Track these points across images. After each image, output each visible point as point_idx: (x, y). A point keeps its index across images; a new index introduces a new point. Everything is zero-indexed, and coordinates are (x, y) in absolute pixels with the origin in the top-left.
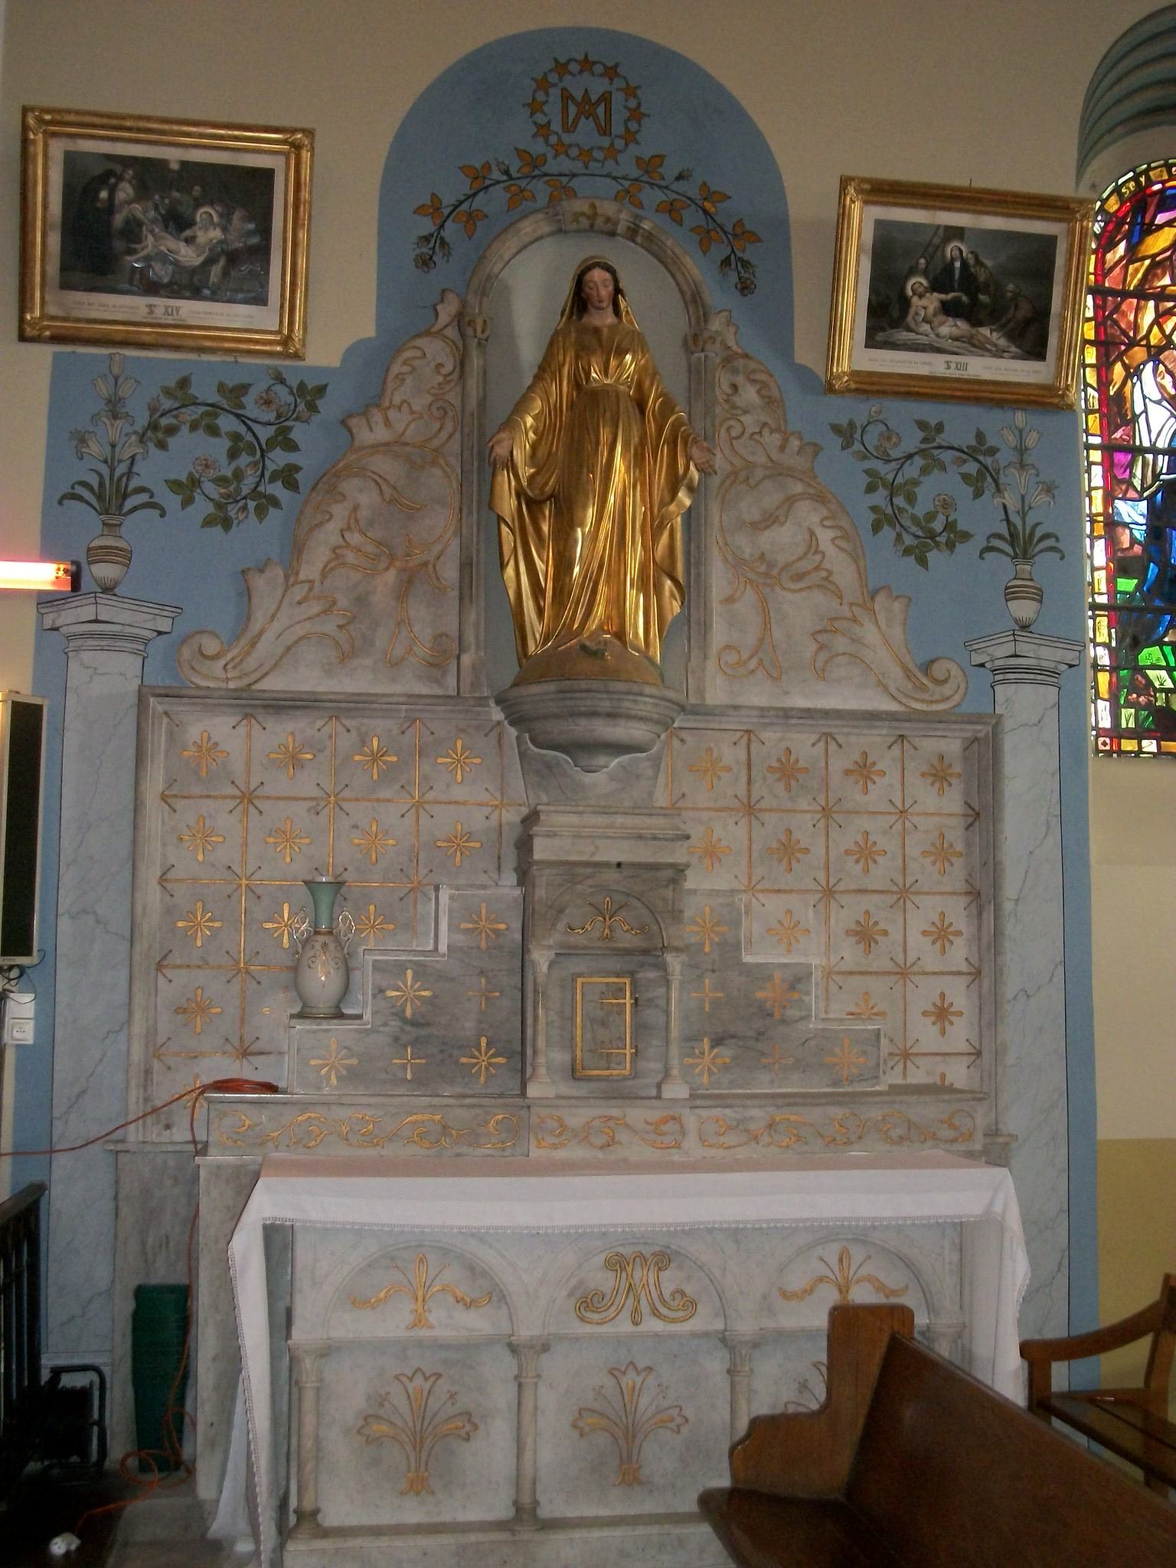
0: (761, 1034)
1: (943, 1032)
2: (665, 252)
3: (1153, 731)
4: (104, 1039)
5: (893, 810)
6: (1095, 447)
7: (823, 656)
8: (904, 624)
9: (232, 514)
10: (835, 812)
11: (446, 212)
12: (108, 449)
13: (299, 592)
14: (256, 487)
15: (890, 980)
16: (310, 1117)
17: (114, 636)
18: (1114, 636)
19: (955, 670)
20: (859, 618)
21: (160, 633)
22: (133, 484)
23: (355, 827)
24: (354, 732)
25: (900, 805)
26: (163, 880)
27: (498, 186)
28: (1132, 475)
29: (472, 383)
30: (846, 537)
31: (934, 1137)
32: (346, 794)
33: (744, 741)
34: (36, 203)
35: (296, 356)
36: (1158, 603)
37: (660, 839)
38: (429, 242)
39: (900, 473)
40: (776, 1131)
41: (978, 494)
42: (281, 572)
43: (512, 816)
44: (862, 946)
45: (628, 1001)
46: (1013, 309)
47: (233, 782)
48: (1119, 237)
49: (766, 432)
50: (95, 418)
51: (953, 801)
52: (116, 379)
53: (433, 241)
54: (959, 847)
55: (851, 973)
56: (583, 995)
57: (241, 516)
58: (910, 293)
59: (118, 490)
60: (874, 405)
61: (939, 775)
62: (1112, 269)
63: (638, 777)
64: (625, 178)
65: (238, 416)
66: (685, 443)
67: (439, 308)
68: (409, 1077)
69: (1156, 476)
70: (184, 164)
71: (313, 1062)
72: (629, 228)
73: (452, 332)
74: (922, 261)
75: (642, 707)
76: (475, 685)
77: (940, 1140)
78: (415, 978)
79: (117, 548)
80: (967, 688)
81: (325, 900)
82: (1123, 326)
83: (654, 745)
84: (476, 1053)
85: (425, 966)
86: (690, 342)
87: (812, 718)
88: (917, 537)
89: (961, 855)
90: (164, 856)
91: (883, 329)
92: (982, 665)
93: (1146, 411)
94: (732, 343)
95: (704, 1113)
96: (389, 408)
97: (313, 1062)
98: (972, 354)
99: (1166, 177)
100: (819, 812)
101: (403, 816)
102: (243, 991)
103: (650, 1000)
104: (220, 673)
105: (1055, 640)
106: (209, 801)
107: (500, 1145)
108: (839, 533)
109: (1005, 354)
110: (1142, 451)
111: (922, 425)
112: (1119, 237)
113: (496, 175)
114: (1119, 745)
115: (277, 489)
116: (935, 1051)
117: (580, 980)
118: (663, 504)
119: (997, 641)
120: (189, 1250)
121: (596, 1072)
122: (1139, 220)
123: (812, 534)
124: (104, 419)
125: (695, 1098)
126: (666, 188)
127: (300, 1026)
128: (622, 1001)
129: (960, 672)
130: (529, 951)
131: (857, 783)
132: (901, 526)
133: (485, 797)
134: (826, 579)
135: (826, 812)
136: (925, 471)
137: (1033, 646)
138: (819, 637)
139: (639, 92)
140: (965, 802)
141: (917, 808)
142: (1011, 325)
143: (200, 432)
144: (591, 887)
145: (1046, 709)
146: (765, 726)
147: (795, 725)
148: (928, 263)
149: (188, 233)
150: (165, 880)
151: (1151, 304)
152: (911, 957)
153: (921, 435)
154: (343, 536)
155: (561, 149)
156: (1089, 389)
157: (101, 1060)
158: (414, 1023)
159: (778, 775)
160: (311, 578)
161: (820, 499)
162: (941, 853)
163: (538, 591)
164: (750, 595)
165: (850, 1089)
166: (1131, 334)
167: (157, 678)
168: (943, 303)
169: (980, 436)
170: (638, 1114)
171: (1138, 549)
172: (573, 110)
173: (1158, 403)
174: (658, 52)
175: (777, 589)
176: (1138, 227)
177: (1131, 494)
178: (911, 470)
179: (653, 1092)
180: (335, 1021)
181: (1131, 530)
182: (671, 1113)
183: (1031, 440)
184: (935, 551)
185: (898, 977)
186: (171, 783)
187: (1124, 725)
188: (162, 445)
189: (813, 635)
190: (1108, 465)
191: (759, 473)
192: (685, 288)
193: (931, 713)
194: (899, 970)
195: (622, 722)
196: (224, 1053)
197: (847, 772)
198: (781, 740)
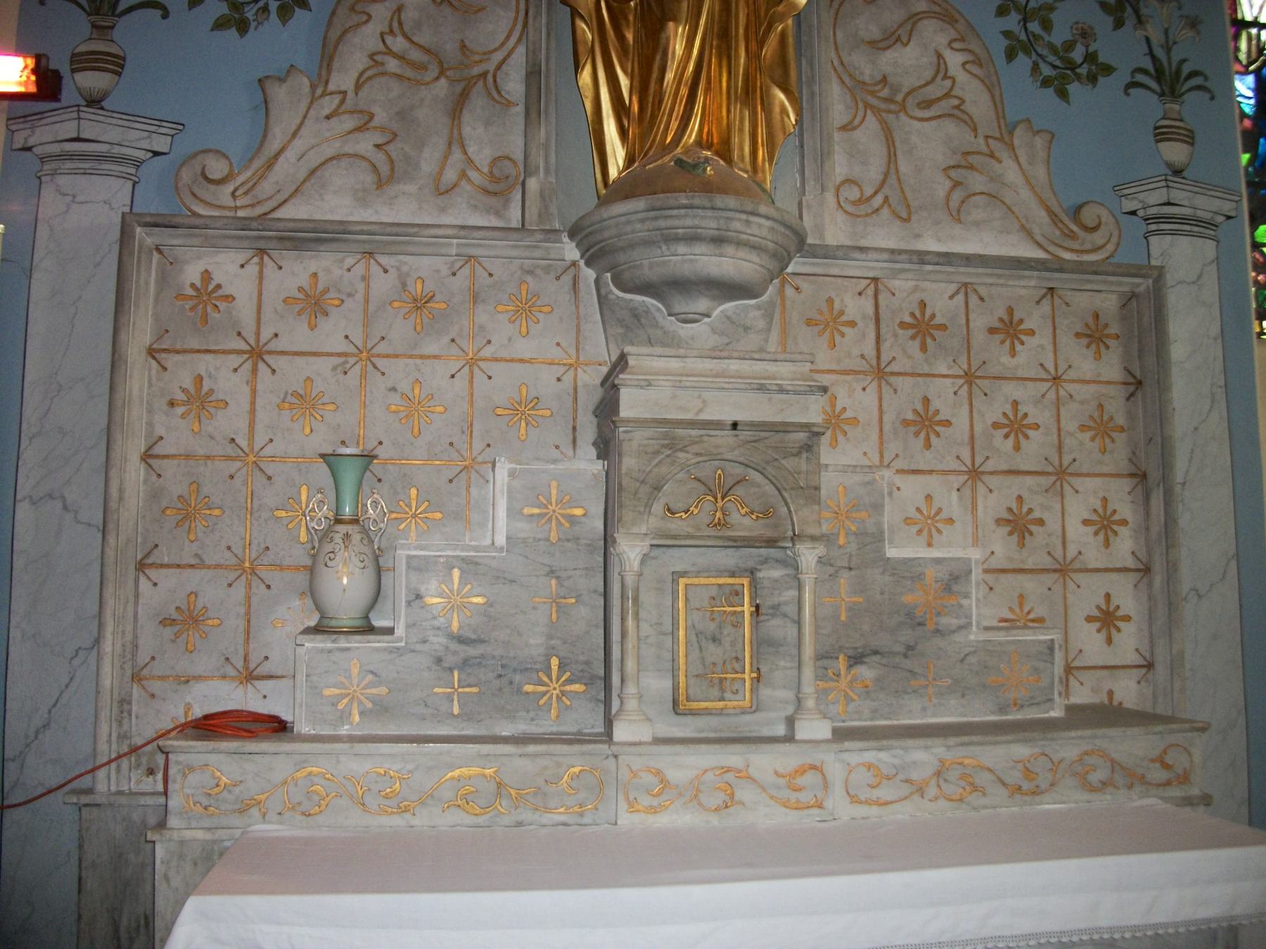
0: (910, 648)
1: (1109, 641)
4: (72, 658)
5: (1044, 376)
7: (957, 196)
8: (1048, 163)
13: (329, 104)
15: (1048, 579)
16: (310, 774)
17: (99, 158)
20: (997, 154)
21: (156, 154)
23: (394, 389)
24: (393, 273)
25: (1053, 371)
26: (147, 457)
30: (978, 62)
31: (1142, 780)
32: (382, 348)
33: (870, 291)
37: (787, 392)
40: (946, 780)
41: (1119, 24)
42: (306, 82)
43: (591, 378)
44: (1015, 537)
45: (747, 609)
47: (239, 334)
51: (1111, 367)
54: (1121, 420)
55: (1003, 571)
56: (687, 600)
61: (1094, 335)
68: (456, 711)
71: (327, 692)
75: (756, 231)
76: (544, 215)
77: (1150, 784)
78: (463, 580)
79: (108, 54)
81: (349, 477)
83: (766, 289)
84: (545, 679)
85: (477, 564)
87: (950, 264)
88: (1055, 67)
89: (1122, 429)
90: (150, 424)
92: (1134, 213)
95: (854, 758)
97: (327, 692)
101: (453, 376)
102: (248, 598)
103: (776, 607)
104: (229, 202)
106: (208, 357)
107: (576, 809)
108: (970, 58)
116: (1101, 663)
117: (682, 581)
121: (704, 705)
123: (939, 56)
125: (841, 735)
127: (314, 643)
128: (739, 609)
129: (1111, 219)
130: (614, 541)
131: (1003, 342)
132: (1037, 54)
133: (556, 353)
134: (957, 107)
135: (969, 377)
137: (1188, 194)
138: (953, 173)
140: (1126, 369)
141: (1072, 374)
144: (697, 454)
146: (895, 274)
150: (151, 456)
152: (1072, 551)
154: (384, 41)
157: (67, 686)
158: (461, 640)
159: (911, 332)
160: (343, 88)
162: (1101, 427)
164: (871, 122)
165: (1019, 717)
167: (150, 204)
170: (765, 762)
175: (902, 116)
179: (781, 730)
180: (358, 637)
182: (809, 761)
184: (1076, 83)
185: (1057, 575)
186: (163, 333)
189: (944, 170)
193: (1081, 263)
194: (1057, 566)
195: (730, 250)
196: (224, 677)
197: (992, 331)
198: (915, 289)
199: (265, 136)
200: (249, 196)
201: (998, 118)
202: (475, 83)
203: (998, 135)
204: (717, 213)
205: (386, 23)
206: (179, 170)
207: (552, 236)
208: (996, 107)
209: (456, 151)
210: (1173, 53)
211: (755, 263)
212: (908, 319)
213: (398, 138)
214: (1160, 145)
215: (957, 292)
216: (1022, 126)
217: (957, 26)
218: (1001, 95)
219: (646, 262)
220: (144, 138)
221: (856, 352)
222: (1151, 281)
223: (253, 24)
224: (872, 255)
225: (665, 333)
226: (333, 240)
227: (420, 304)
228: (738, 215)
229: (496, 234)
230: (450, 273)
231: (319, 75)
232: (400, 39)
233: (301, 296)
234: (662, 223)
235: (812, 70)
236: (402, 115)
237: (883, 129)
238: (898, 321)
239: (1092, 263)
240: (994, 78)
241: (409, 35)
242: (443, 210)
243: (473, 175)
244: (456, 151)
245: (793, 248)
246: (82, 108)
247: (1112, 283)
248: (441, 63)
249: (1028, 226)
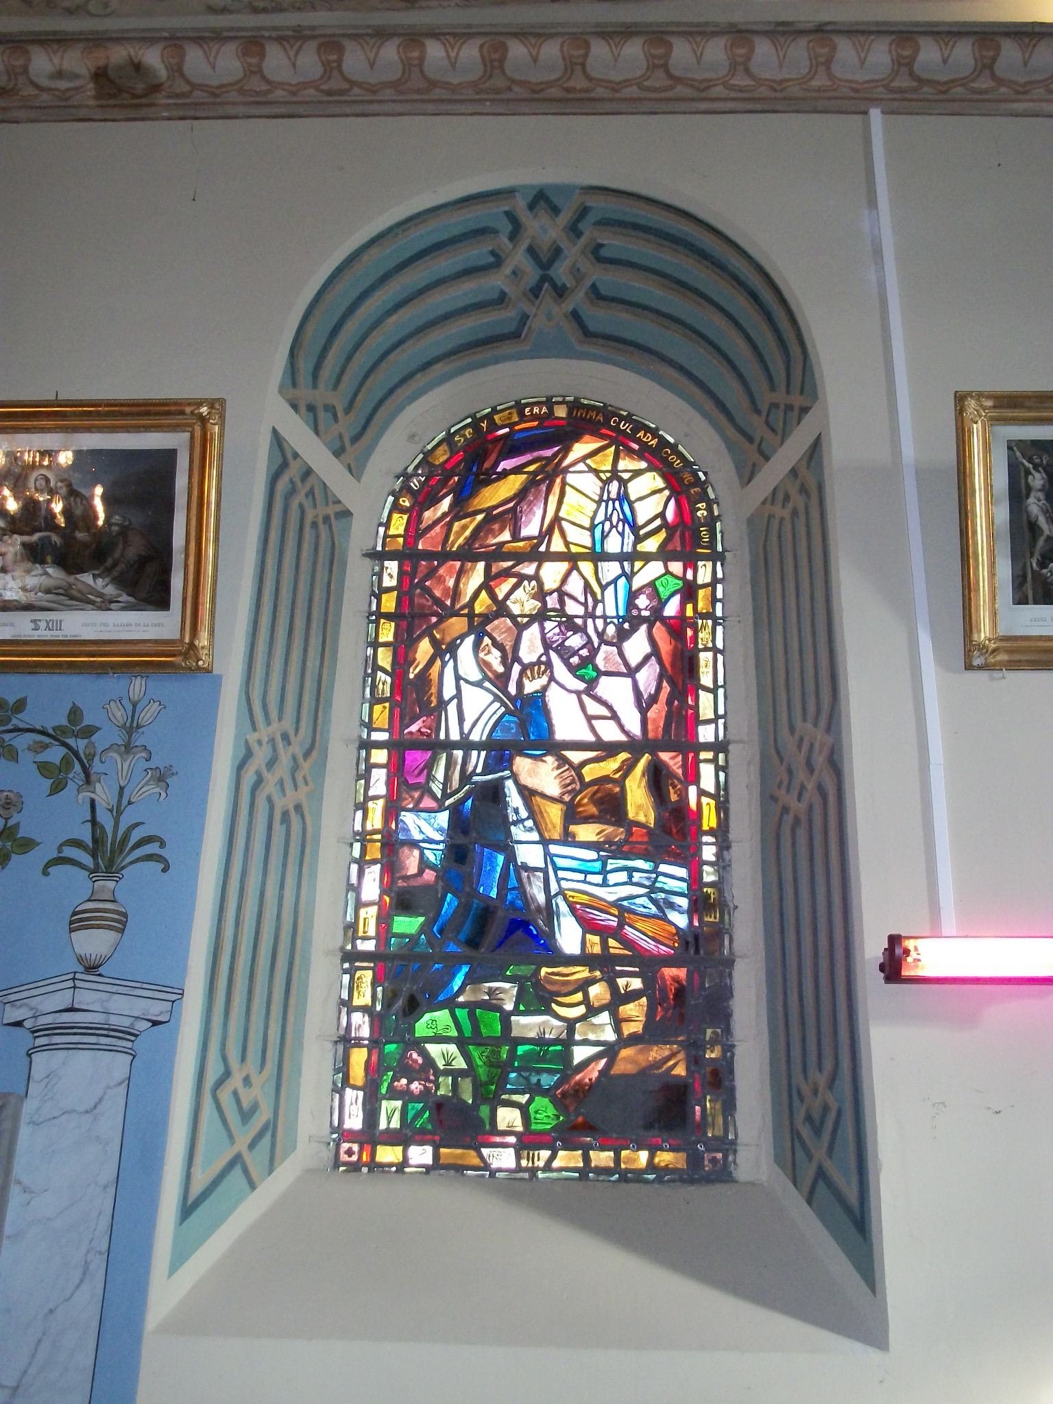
3: (430, 1132)
6: (379, 745)
18: (380, 995)
28: (430, 777)
36: (452, 948)
46: (121, 546)
48: (445, 491)
62: (430, 528)
69: (465, 778)
82: (438, 593)
92: (19, 1024)
93: (458, 695)
98: (70, 608)
99: (515, 418)
105: (130, 985)
109: (113, 606)
110: (449, 746)
112: (445, 491)
114: (373, 1154)
122: (475, 469)
145: (109, 1087)
151: (481, 566)
156: (379, 674)
166: (448, 603)
171: (429, 876)
173: (478, 684)
177: (428, 802)
181: (422, 850)
183: (146, 716)
187: (383, 1125)
190: (396, 768)
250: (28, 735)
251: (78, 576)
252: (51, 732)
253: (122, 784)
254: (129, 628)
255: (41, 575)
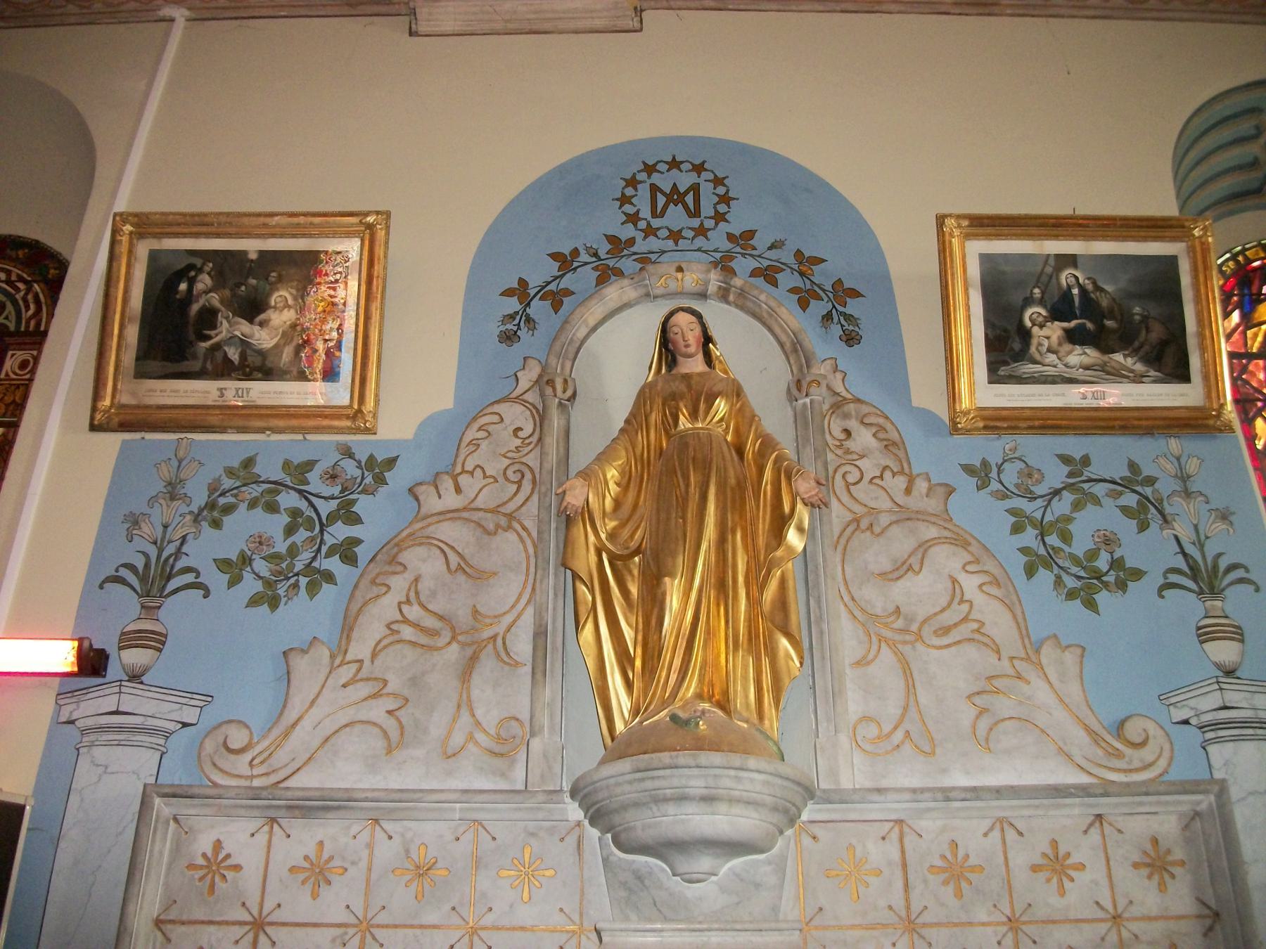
2: (760, 306)
5: (1101, 914)
7: (983, 725)
9: (281, 592)
10: (1025, 923)
11: (532, 292)
12: (160, 529)
13: (346, 673)
14: (311, 563)
19: (1152, 729)
20: (1024, 674)
21: (185, 725)
22: (180, 564)
24: (397, 839)
27: (587, 267)
29: (552, 441)
30: (996, 582)
33: (895, 835)
34: (116, 299)
35: (368, 431)
38: (514, 319)
39: (1049, 509)
41: (1143, 527)
42: (327, 653)
47: (244, 904)
49: (888, 474)
50: (152, 500)
52: (180, 462)
53: (518, 317)
57: (291, 593)
58: (1028, 323)
59: (161, 575)
60: (1006, 442)
63: (757, 886)
64: (716, 251)
65: (300, 492)
66: (789, 478)
67: (519, 374)
70: (262, 254)
72: (720, 287)
73: (532, 397)
74: (1037, 291)
75: (748, 786)
80: (1172, 750)
82: (1255, 385)
86: (795, 392)
87: (978, 798)
88: (1079, 578)
91: (1006, 363)
92: (1186, 722)
94: (840, 388)
96: (461, 474)
100: (1004, 924)
106: (212, 928)
109: (1144, 379)
111: (1066, 459)
113: (584, 257)
115: (334, 564)
118: (770, 549)
119: (1199, 692)
120: (1009, 882)
123: (954, 581)
124: (162, 501)
126: (759, 256)
129: (1160, 732)
131: (1048, 880)
132: (1059, 566)
133: (559, 919)
134: (978, 631)
136: (1077, 506)
138: (977, 700)
139: (726, 181)
140: (1198, 899)
142: (1146, 348)
143: (259, 511)
147: (958, 809)
148: (1043, 293)
149: (262, 317)
153: (1066, 469)
154: (400, 610)
155: (650, 232)
160: (359, 657)
161: (960, 541)
163: (624, 659)
167: (175, 775)
168: (1066, 331)
169: (1133, 466)
172: (661, 200)
174: (743, 150)
175: (919, 646)
176: (1247, 297)
178: (1062, 506)
183: (1192, 466)
184: (1104, 593)
188: (216, 524)
189: (969, 697)
191: (884, 519)
192: (783, 338)
195: (723, 807)
197: (1035, 868)
199: (284, 706)
200: (265, 765)
201: (1022, 639)
202: (486, 646)
203: (1023, 655)
204: (703, 771)
205: (404, 593)
206: (204, 739)
207: (554, 797)
208: (1019, 628)
209: (465, 714)
210: (1206, 549)
211: (755, 819)
212: (939, 863)
213: (409, 704)
214: (1206, 646)
215: (991, 829)
216: (1049, 642)
217: (970, 548)
218: (1023, 613)
219: (638, 824)
220: (176, 710)
221: (882, 903)
222: (1212, 798)
223: (284, 600)
224: (891, 796)
225: (670, 895)
226: (338, 808)
227: (422, 871)
228: (726, 772)
229: (499, 797)
230: (453, 838)
231: (339, 647)
232: (416, 608)
233: (306, 865)
234: (649, 784)
235: (820, 607)
236: (414, 681)
237: (899, 660)
238: (927, 865)
239: (1144, 783)
240: (1014, 598)
241: (425, 604)
242: (449, 773)
243: (480, 737)
244: (465, 714)
245: (798, 801)
246: (123, 683)
247: (1167, 803)
248: (453, 629)
249: (1065, 749)
250: (1102, 484)
251: (1111, 355)
252: (1119, 481)
253: (1195, 522)
254: (1160, 397)
255: (1081, 355)
